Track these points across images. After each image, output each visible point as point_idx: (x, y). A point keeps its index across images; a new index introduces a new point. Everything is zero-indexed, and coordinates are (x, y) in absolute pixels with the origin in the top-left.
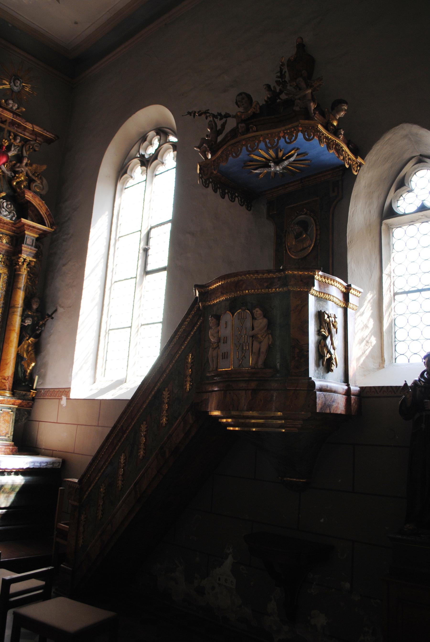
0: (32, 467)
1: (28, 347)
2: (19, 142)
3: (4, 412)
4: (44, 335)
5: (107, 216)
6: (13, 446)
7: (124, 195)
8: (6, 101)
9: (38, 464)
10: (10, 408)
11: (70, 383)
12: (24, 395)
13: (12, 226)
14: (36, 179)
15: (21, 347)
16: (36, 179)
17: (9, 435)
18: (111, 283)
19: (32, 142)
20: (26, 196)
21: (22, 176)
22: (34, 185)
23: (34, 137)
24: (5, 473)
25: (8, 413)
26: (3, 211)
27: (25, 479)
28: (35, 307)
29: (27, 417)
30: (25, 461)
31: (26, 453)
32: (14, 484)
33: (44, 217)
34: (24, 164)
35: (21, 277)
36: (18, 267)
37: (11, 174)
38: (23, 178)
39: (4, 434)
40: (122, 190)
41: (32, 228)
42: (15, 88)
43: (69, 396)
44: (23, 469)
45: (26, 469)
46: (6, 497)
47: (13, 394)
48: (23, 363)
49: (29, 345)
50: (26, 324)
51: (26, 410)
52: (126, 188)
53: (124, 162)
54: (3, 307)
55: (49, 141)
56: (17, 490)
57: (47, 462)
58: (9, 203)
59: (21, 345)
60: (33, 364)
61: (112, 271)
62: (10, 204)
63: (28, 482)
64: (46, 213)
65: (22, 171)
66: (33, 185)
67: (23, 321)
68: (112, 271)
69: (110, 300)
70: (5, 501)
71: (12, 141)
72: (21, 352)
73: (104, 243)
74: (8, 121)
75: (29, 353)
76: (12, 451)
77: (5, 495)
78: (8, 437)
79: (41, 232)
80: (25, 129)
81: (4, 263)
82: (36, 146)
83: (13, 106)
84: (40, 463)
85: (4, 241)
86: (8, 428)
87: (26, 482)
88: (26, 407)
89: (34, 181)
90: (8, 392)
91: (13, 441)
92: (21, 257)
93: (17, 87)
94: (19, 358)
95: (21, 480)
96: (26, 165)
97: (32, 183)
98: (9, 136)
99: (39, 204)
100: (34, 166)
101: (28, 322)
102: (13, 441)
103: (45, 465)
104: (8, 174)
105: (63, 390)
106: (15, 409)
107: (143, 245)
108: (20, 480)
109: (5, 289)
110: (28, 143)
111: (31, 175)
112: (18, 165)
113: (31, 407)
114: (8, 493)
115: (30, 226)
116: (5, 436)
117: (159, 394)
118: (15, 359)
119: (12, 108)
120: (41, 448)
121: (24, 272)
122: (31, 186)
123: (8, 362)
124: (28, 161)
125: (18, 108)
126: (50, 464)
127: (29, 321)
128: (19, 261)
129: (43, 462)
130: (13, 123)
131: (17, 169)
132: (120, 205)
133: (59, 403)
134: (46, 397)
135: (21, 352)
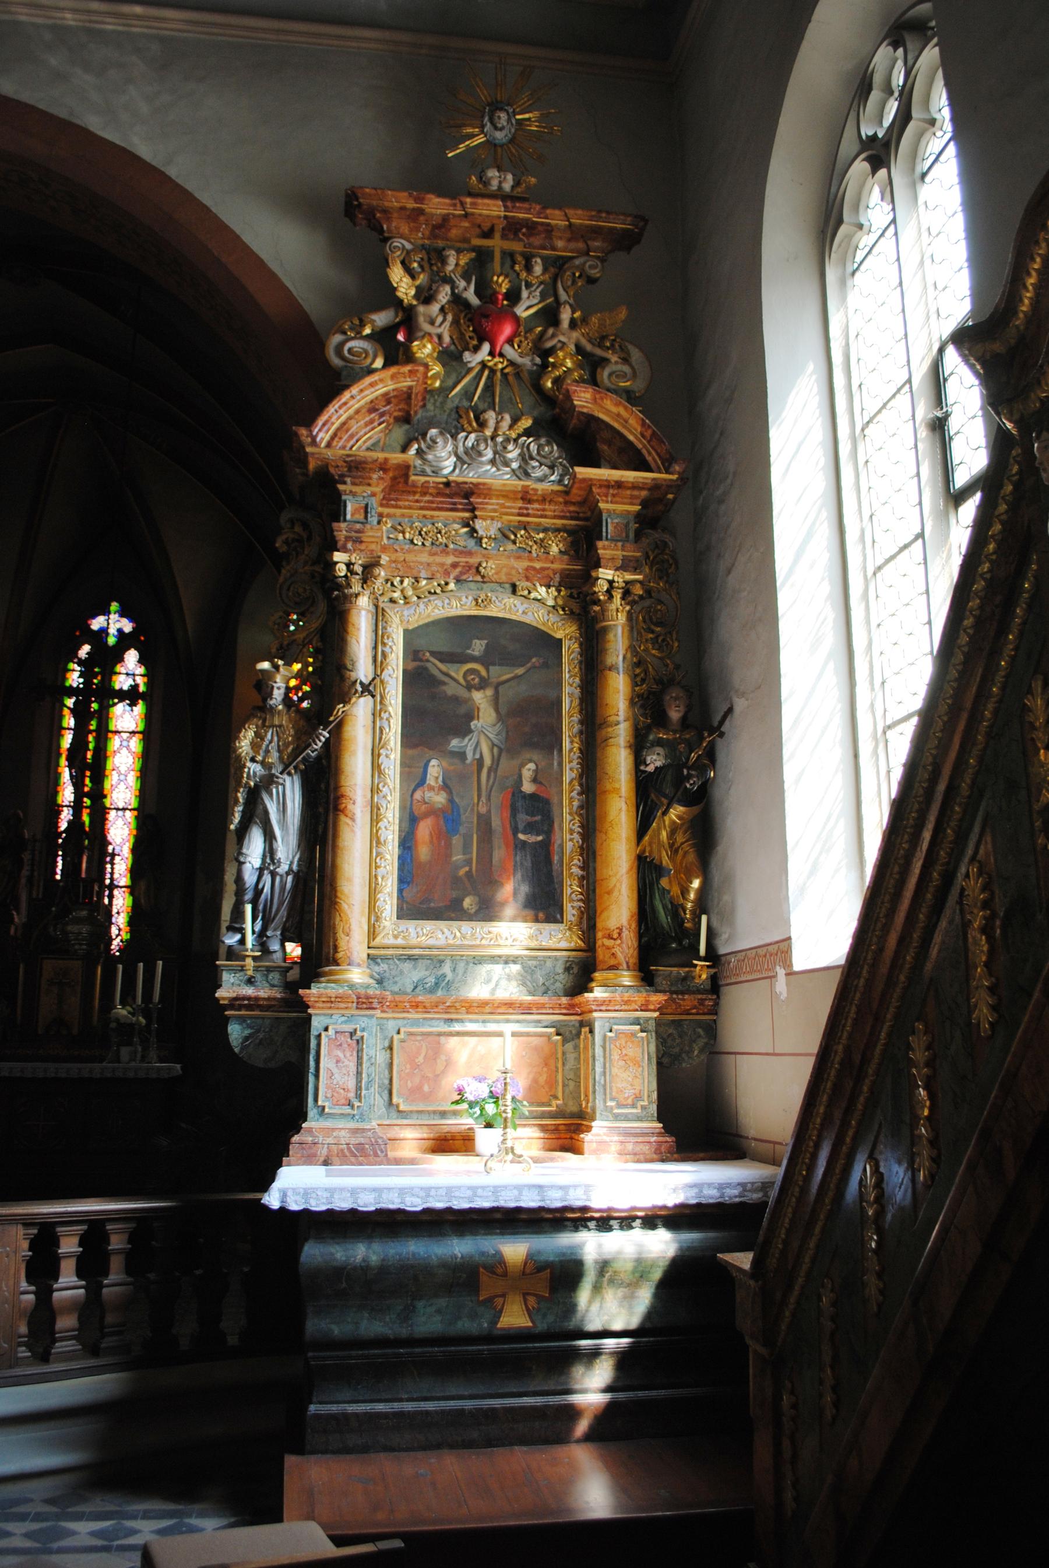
0: (693, 1201)
1: (672, 833)
2: (543, 274)
3: (619, 1033)
4: (717, 792)
5: (814, 377)
6: (659, 1134)
7: (853, 298)
8: (480, 179)
9: (714, 1192)
10: (636, 1022)
11: (787, 923)
12: (684, 979)
13: (566, 503)
14: (609, 355)
15: (651, 838)
16: (609, 355)
17: (646, 1103)
18: (865, 576)
19: (577, 262)
20: (576, 403)
21: (565, 358)
22: (606, 373)
23: (581, 245)
24: (612, 1222)
25: (633, 1034)
26: (534, 467)
27: (679, 1242)
28: (675, 714)
29: (706, 1044)
30: (680, 1182)
31: (702, 1155)
32: (644, 1256)
33: (640, 446)
34: (565, 323)
35: (611, 636)
36: (597, 608)
37: (532, 360)
38: (569, 363)
39: (630, 1101)
40: (843, 283)
41: (617, 488)
42: (499, 135)
43: (791, 965)
44: (664, 1207)
45: (676, 1206)
46: (625, 1297)
47: (647, 978)
48: (664, 882)
49: (674, 830)
50: (651, 768)
51: (699, 1024)
52: (853, 273)
53: (829, 195)
54: (581, 732)
55: (625, 241)
56: (657, 1275)
57: (743, 1185)
58: (543, 441)
59: (650, 832)
60: (696, 884)
61: (862, 538)
62: (548, 443)
63: (689, 1248)
64: (643, 436)
65: (564, 344)
66: (604, 375)
67: (639, 760)
68: (862, 538)
69: (869, 632)
70: (623, 1311)
71: (524, 275)
72: (651, 852)
73: (820, 458)
74: (501, 225)
75: (677, 851)
76: (658, 1151)
77: (621, 1292)
78: (643, 1108)
79: (644, 493)
80: (549, 230)
81: (563, 610)
82: (591, 267)
83: (500, 182)
84: (721, 1187)
85: (554, 550)
86: (637, 1082)
87: (681, 1249)
88: (697, 1014)
89: (605, 361)
90: (625, 973)
91: (659, 1120)
92: (598, 578)
93: (501, 129)
94: (647, 870)
95: (666, 1242)
96: (573, 324)
97: (599, 370)
98: (512, 267)
99: (619, 415)
100: (594, 320)
101: (655, 760)
102: (660, 1119)
103: (736, 1192)
104: (525, 365)
105: (776, 947)
106: (652, 1025)
107: (924, 411)
108: (661, 1245)
109: (577, 680)
110: (566, 266)
111: (589, 347)
112: (551, 331)
113: (715, 1011)
114: (629, 1285)
115: (607, 485)
116: (634, 1106)
117: (939, 887)
118: (635, 870)
119: (500, 188)
120: (747, 1138)
121: (618, 618)
122: (598, 377)
123: (611, 885)
124: (573, 312)
125: (517, 184)
126: (752, 1191)
127: (654, 757)
128: (596, 589)
129: (729, 1185)
130: (513, 228)
131: (549, 344)
132: (847, 327)
133: (772, 987)
134: (743, 978)
135: (651, 852)
